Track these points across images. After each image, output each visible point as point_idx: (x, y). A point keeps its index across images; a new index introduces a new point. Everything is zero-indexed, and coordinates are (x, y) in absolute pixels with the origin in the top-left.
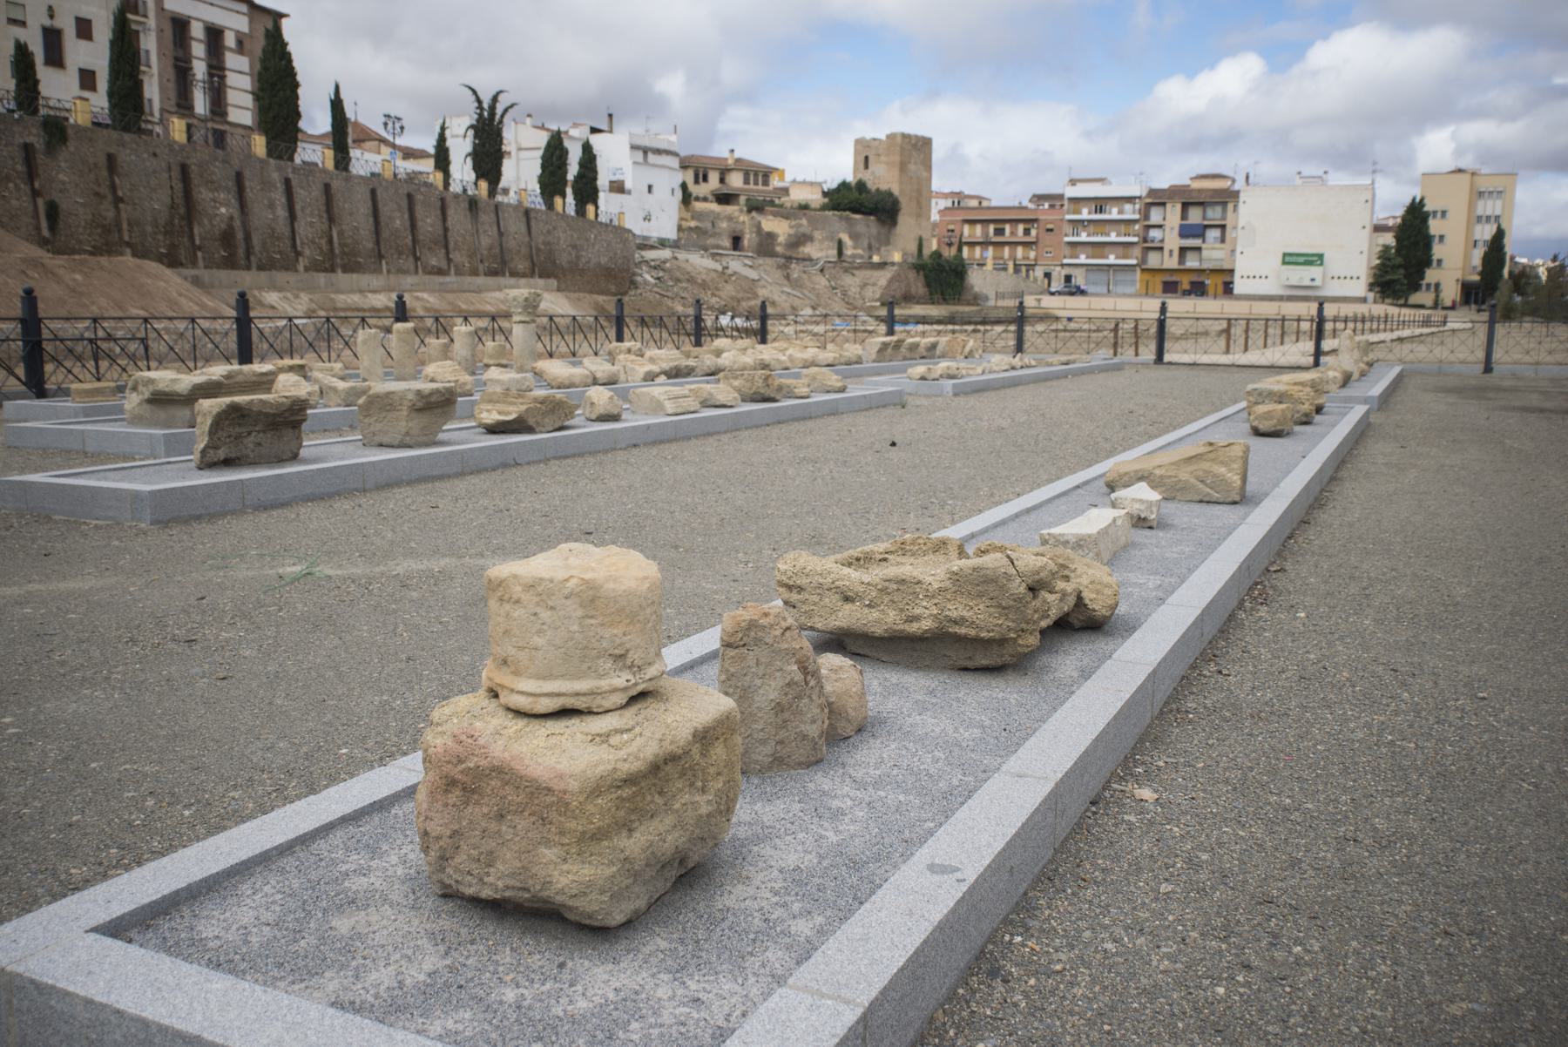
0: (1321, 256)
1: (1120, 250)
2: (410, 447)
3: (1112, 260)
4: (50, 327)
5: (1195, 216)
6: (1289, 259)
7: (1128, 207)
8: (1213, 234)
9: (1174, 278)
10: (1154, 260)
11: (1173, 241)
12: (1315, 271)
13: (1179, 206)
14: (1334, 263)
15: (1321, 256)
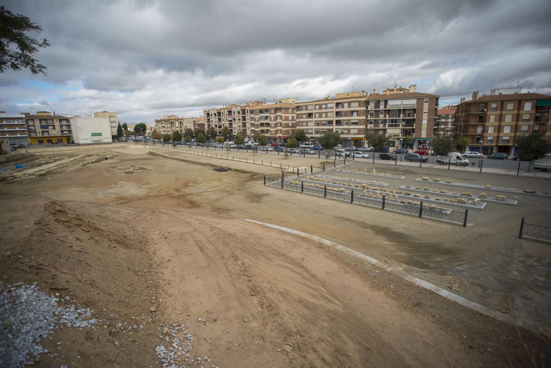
0: (101, 134)
1: (21, 133)
2: (411, 161)
3: (19, 135)
4: (525, 222)
5: (44, 123)
6: (93, 135)
7: (20, 120)
8: (50, 127)
9: (41, 139)
10: (33, 135)
11: (39, 130)
12: (100, 137)
13: (38, 121)
14: (104, 135)
15: (101, 134)
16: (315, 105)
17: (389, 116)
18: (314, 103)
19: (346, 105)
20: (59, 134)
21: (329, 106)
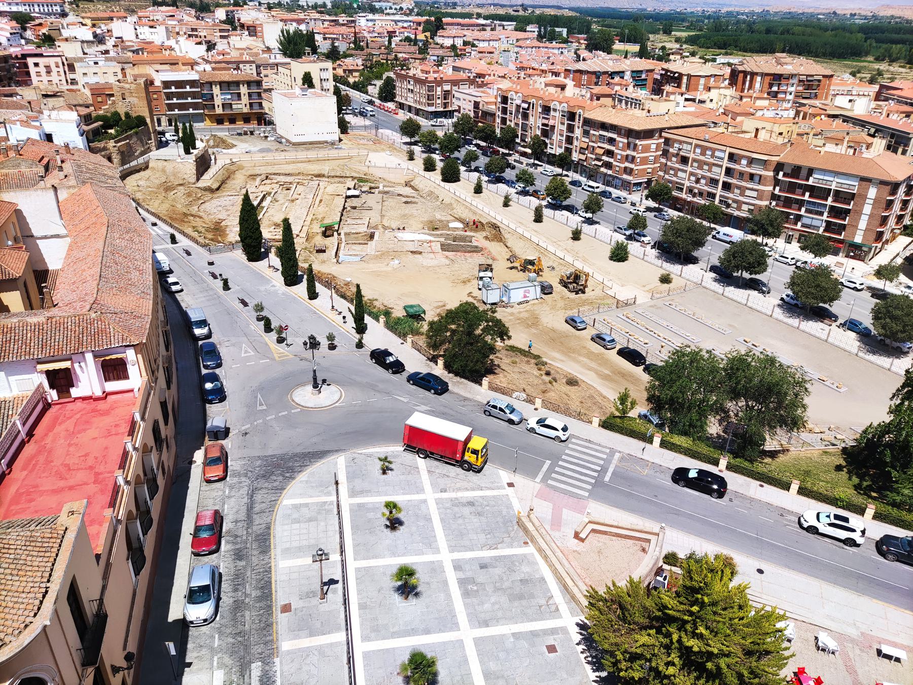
16: (697, 146)
17: (810, 196)
18: (695, 142)
19: (744, 162)
20: (246, 110)
21: (717, 154)
